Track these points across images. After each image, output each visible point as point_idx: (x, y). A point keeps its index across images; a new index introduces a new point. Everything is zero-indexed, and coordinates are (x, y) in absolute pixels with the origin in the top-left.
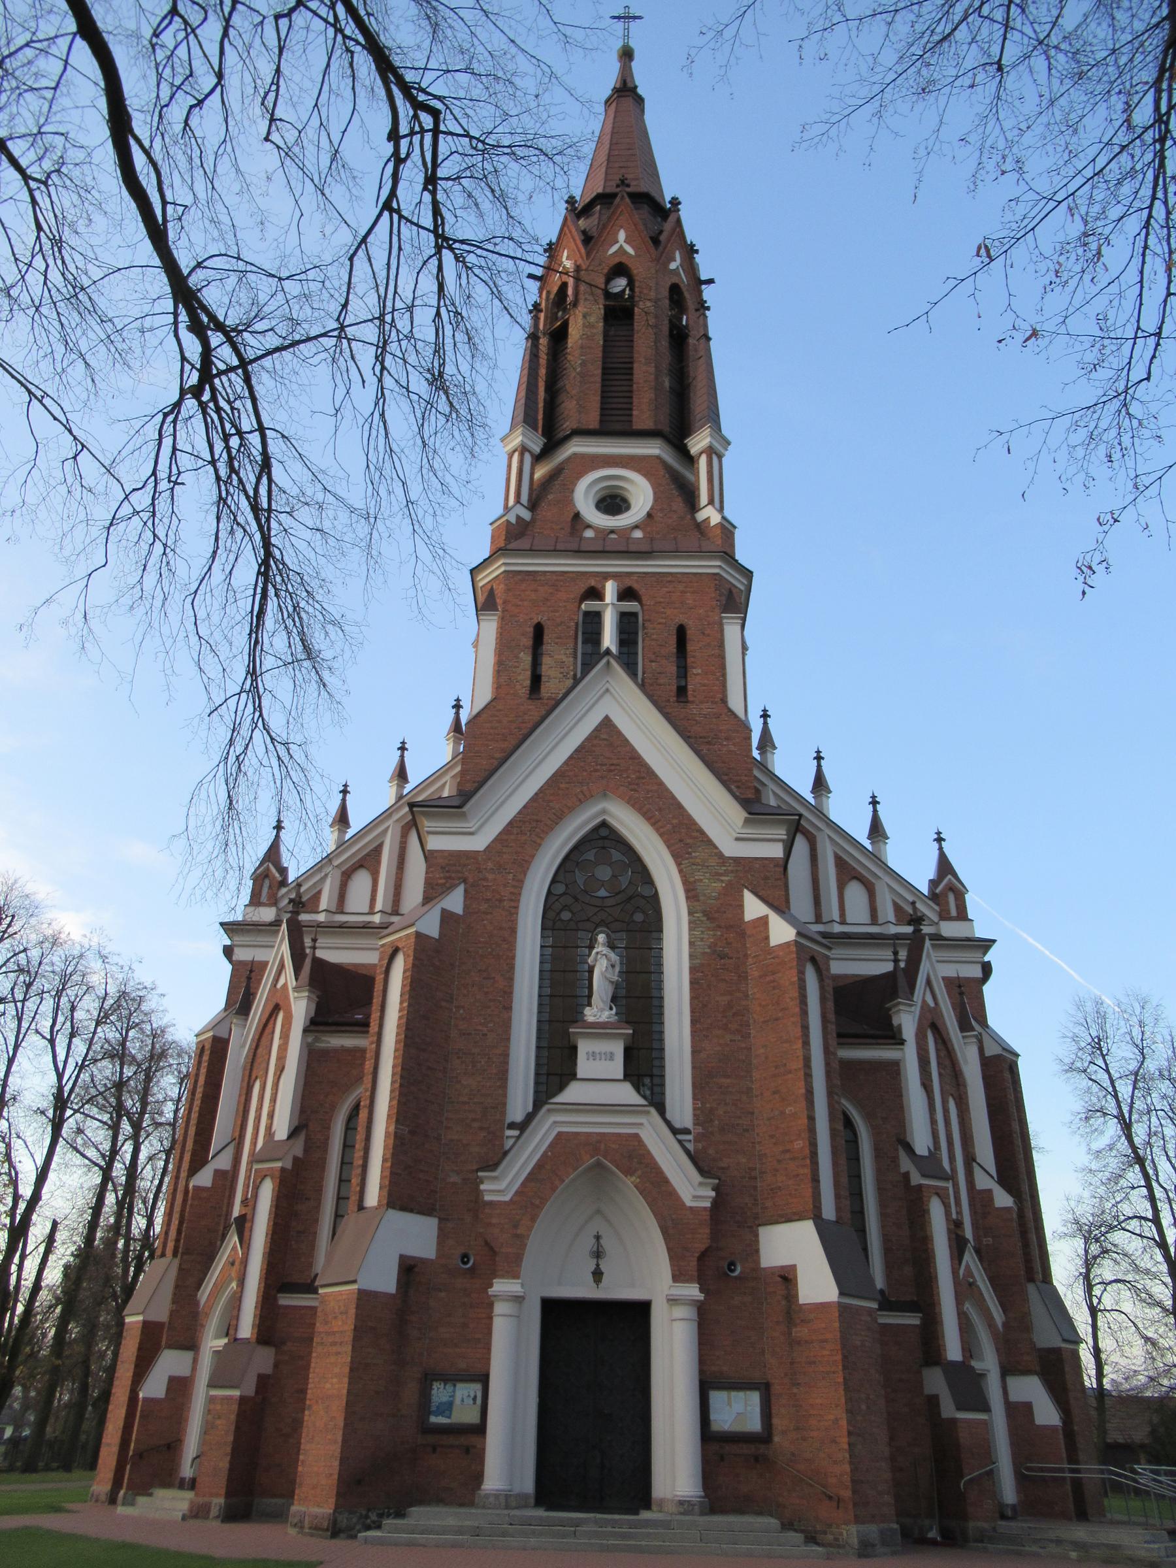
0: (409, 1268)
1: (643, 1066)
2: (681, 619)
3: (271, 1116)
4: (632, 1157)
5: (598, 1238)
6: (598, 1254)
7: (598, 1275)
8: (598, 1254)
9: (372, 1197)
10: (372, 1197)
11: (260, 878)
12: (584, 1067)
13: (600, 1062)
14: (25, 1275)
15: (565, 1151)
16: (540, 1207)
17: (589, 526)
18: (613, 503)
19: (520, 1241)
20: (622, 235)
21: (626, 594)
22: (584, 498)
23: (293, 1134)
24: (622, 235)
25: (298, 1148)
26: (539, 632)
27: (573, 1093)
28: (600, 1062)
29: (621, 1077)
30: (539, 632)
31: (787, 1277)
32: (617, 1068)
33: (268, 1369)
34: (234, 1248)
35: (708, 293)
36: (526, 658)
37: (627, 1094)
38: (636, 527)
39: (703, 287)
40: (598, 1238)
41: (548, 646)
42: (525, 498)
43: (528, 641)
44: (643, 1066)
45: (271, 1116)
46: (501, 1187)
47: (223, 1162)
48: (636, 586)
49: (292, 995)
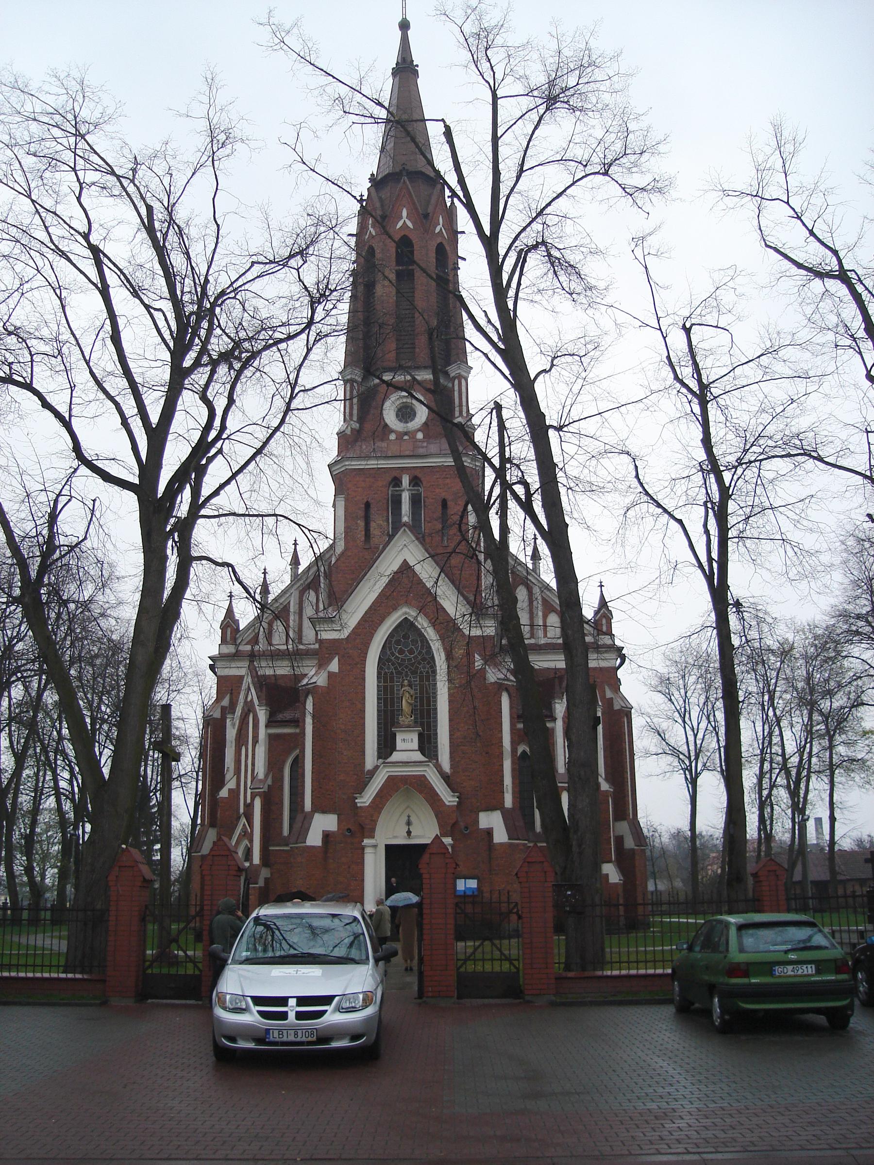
0: (327, 836)
1: (427, 745)
2: (444, 495)
3: (253, 764)
4: (421, 785)
5: (409, 817)
6: (409, 823)
7: (409, 833)
8: (409, 823)
9: (308, 805)
10: (308, 805)
11: (224, 627)
12: (399, 745)
13: (407, 743)
14: (643, 1157)
15: (393, 785)
16: (382, 808)
17: (392, 431)
18: (405, 413)
19: (374, 822)
20: (405, 213)
21: (415, 481)
22: (390, 416)
23: (266, 776)
24: (405, 213)
25: (269, 781)
26: (367, 505)
27: (395, 757)
28: (407, 743)
29: (417, 748)
30: (367, 505)
31: (489, 832)
32: (415, 745)
33: (269, 876)
34: (244, 825)
35: (461, 263)
36: (361, 523)
37: (418, 756)
38: (419, 430)
39: (459, 235)
40: (409, 817)
41: (373, 510)
42: (355, 418)
43: (361, 513)
44: (427, 745)
45: (253, 764)
46: (366, 799)
47: (231, 784)
48: (419, 475)
49: (257, 708)
